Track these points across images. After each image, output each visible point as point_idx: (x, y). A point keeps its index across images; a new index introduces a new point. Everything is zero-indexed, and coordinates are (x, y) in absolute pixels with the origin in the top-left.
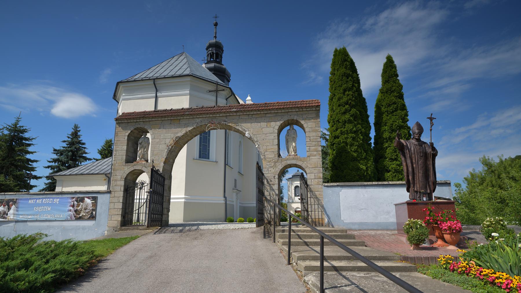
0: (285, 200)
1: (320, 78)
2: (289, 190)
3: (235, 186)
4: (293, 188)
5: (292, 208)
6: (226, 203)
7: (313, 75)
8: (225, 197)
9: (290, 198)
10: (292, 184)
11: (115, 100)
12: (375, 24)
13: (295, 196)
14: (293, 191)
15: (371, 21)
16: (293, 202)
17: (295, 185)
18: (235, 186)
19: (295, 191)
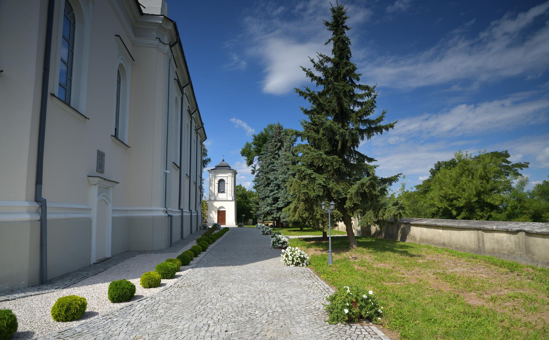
0: (206, 196)
1: (244, 63)
2: (210, 184)
3: (100, 167)
4: (217, 182)
5: (213, 207)
6: (43, 221)
7: (236, 58)
8: (39, 198)
9: (211, 194)
10: (215, 177)
11: (69, 105)
12: (304, 9)
13: (219, 192)
14: (217, 185)
15: (300, 6)
16: (215, 200)
17: (219, 178)
18: (100, 167)
19: (219, 186)
